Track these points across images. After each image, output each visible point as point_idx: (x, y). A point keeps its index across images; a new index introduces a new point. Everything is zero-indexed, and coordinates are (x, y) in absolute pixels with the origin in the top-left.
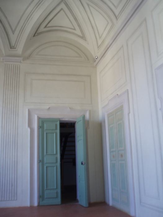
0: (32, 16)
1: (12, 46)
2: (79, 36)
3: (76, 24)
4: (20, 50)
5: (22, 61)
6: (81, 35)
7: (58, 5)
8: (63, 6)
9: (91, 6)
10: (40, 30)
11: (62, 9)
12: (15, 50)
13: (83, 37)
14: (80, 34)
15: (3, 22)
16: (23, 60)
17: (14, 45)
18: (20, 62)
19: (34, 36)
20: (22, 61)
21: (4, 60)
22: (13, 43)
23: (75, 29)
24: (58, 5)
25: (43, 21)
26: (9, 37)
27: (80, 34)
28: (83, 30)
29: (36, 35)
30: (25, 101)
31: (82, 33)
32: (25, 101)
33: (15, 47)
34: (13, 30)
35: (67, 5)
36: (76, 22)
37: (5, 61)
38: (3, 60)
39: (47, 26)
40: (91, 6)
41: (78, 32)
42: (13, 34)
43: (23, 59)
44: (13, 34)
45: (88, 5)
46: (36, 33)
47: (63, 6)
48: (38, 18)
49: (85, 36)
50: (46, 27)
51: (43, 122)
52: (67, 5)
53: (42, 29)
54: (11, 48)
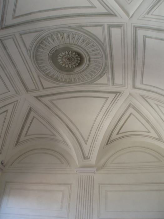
0: (102, 124)
1: (85, 156)
2: (156, 139)
3: (149, 126)
4: (93, 160)
5: (96, 172)
6: (157, 137)
7: (126, 110)
8: (131, 110)
9: (160, 106)
10: (112, 139)
11: (131, 114)
12: (88, 160)
13: (160, 139)
14: (155, 136)
15: (75, 134)
16: (97, 170)
17: (87, 156)
18: (94, 173)
19: (107, 144)
20: (96, 172)
21: (78, 172)
22: (86, 153)
23: (149, 132)
24: (126, 110)
25: (114, 128)
26: (82, 147)
27: (155, 136)
28: (158, 131)
29: (109, 143)
30: (99, 217)
31: (158, 135)
32: (99, 217)
33: (89, 157)
34: (86, 140)
35: (134, 108)
36: (149, 124)
37: (79, 173)
38: (77, 171)
39: (120, 133)
40: (160, 106)
41: (153, 134)
42: (150, 133)
43: (97, 169)
44: (150, 133)
45: (157, 105)
46: (109, 141)
47: (131, 110)
48: (108, 126)
49: (161, 138)
50: (118, 134)
51: (17, 93)
52: (134, 108)
53: (114, 136)
54: (84, 158)
